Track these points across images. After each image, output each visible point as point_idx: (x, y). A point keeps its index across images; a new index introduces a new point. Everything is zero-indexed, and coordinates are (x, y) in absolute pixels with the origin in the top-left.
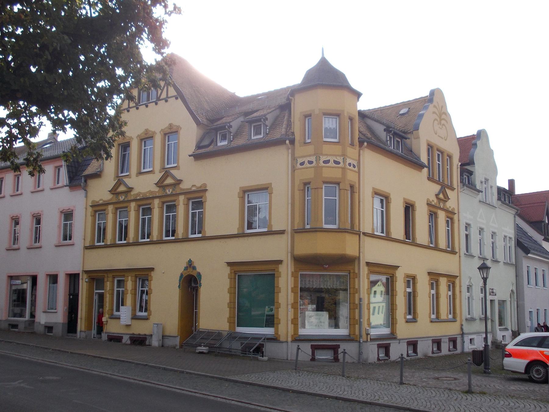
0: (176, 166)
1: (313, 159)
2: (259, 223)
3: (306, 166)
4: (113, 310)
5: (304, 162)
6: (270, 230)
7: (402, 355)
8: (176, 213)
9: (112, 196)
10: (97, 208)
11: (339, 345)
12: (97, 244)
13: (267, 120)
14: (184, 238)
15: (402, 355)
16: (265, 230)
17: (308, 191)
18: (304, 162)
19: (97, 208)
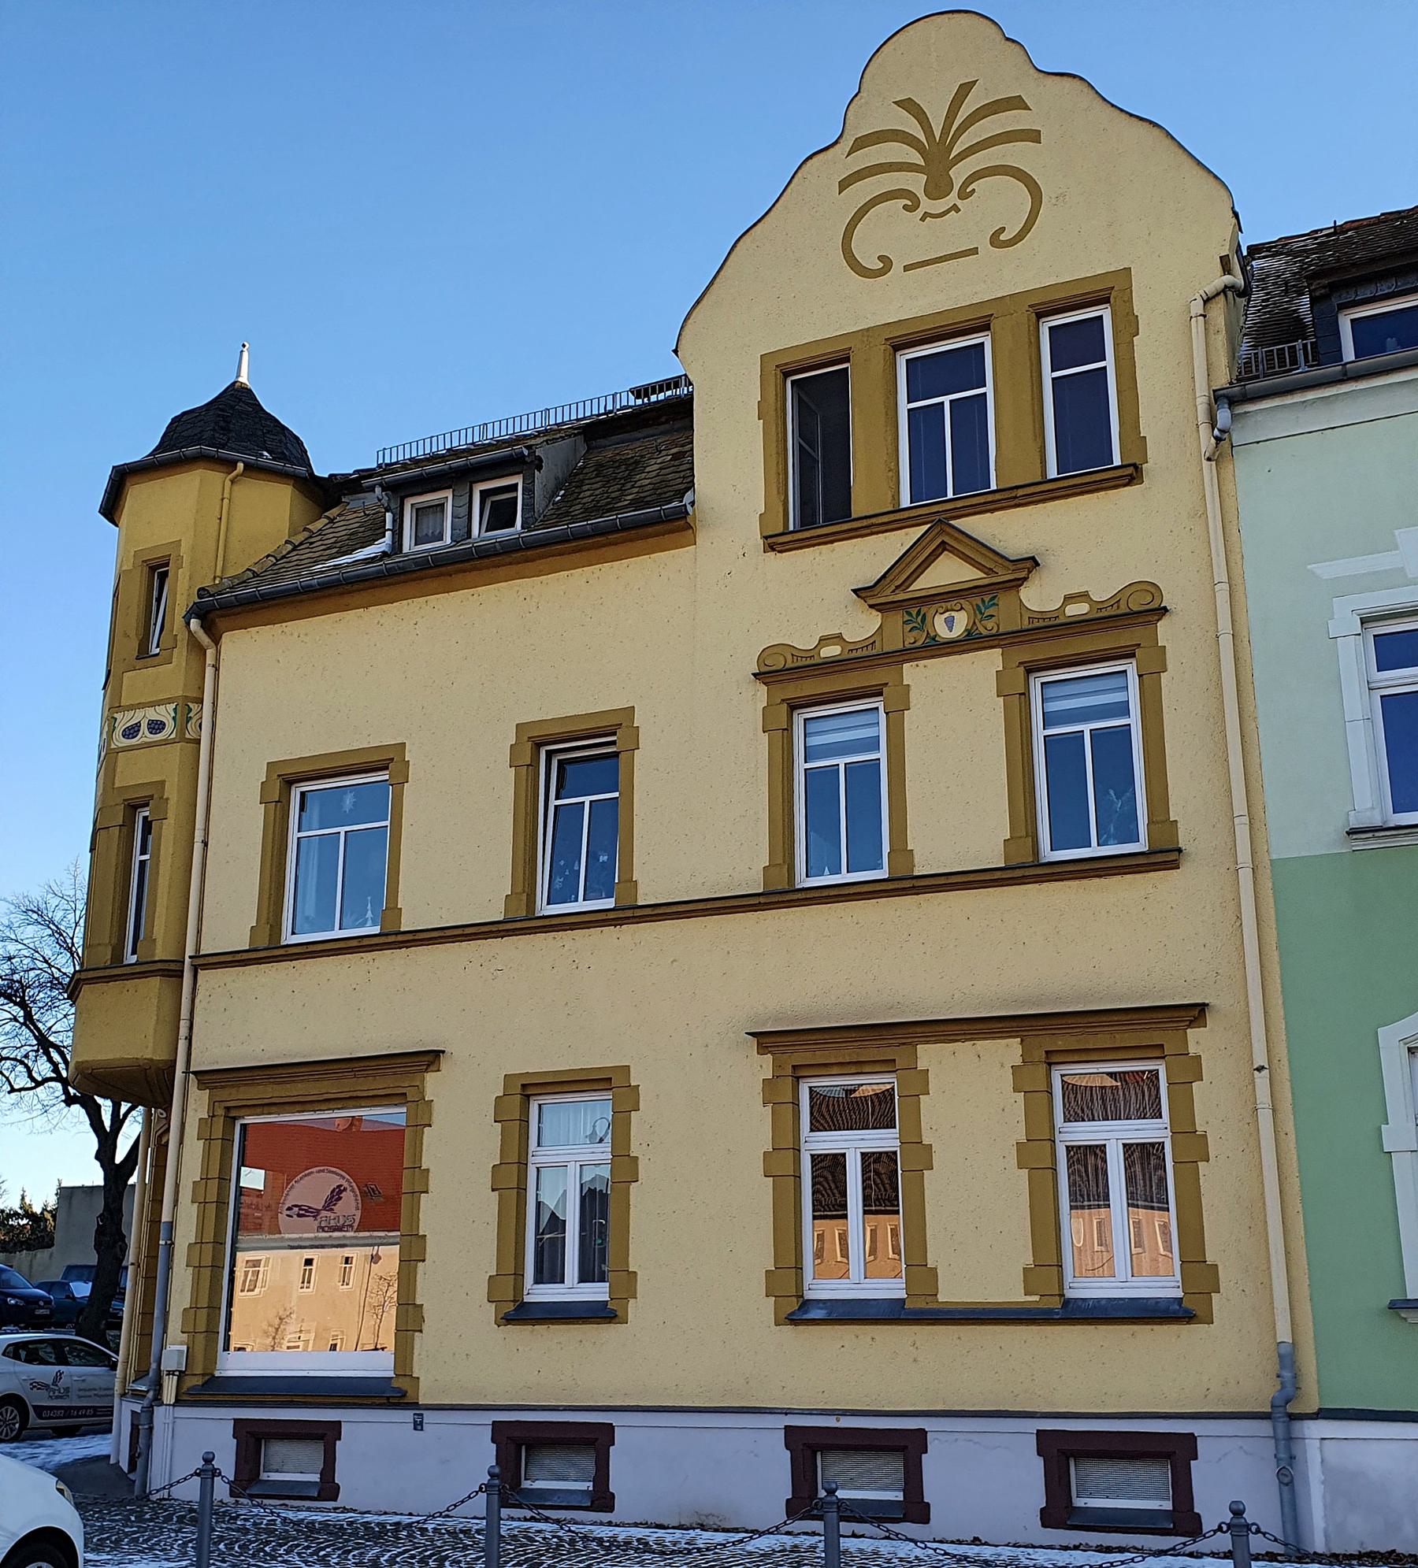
0: (159, 653)
1: (165, 713)
2: (621, 874)
3: (144, 739)
4: (519, 1275)
5: (138, 725)
6: (628, 903)
7: (208, 1459)
8: (616, 794)
9: (874, 620)
10: (794, 691)
11: (337, 1425)
12: (1049, 855)
13: (539, 468)
14: (1013, 863)
15: (208, 1459)
16: (609, 903)
17: (302, 808)
18: (138, 725)
19: (794, 691)
